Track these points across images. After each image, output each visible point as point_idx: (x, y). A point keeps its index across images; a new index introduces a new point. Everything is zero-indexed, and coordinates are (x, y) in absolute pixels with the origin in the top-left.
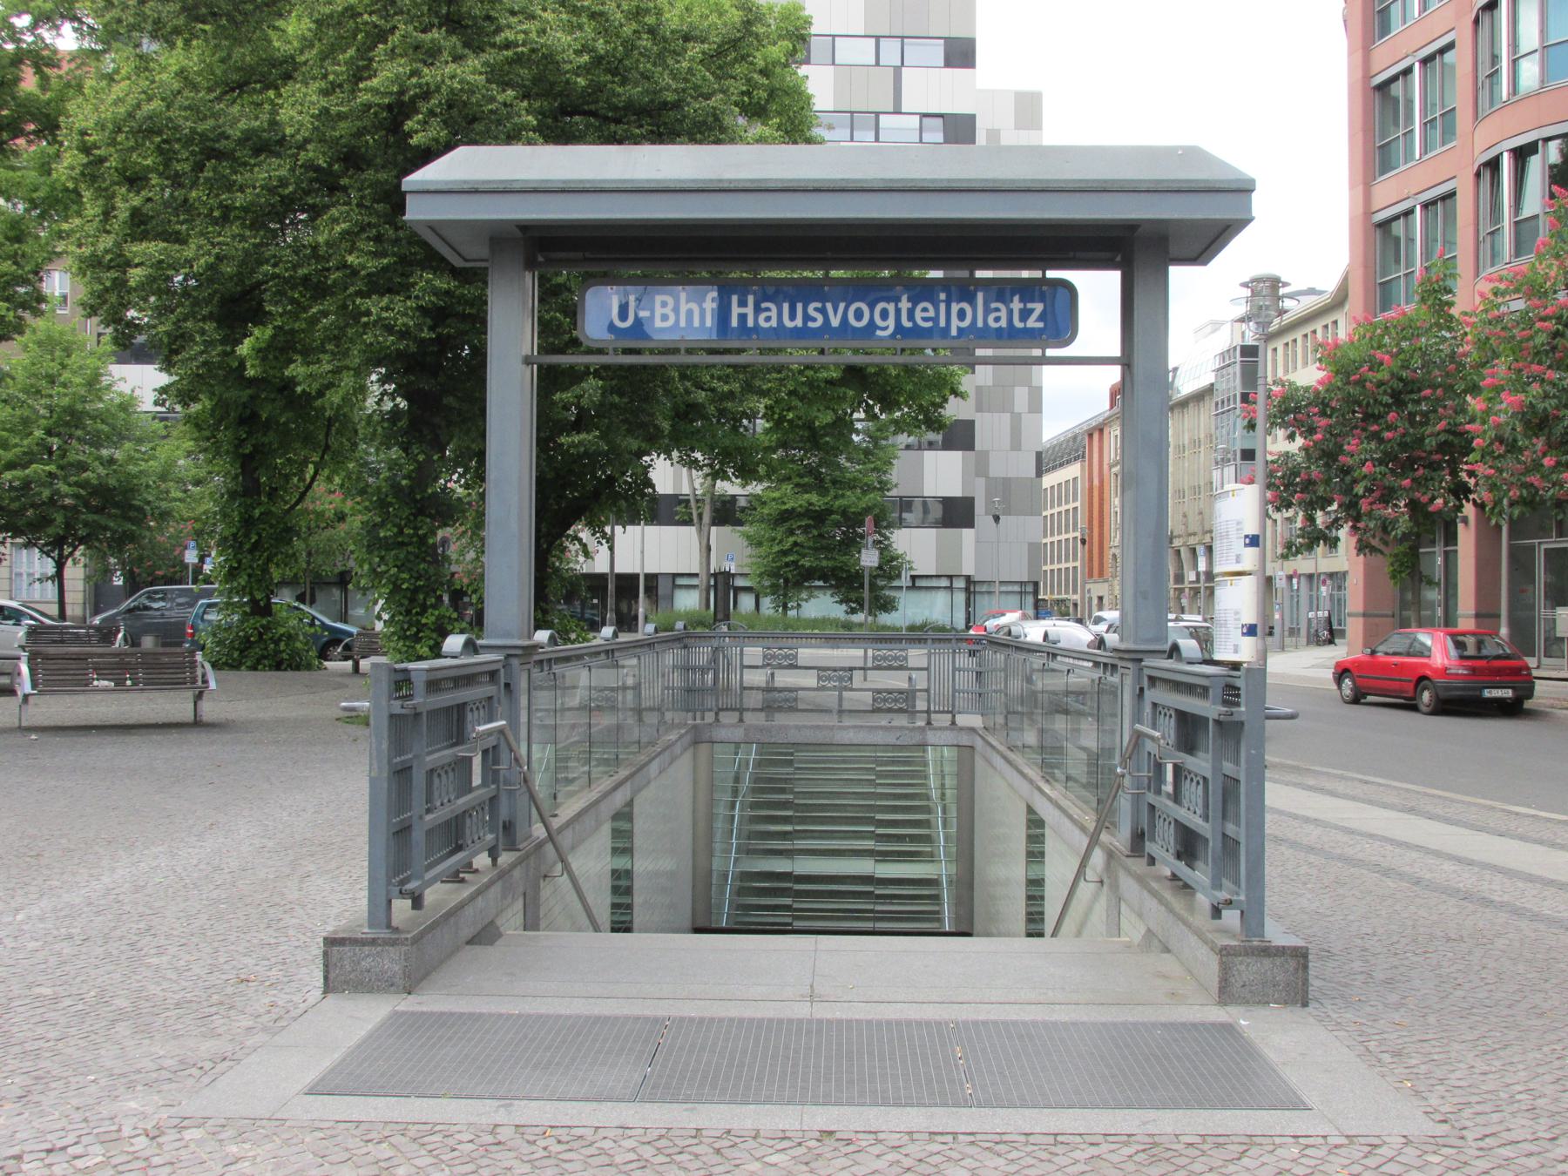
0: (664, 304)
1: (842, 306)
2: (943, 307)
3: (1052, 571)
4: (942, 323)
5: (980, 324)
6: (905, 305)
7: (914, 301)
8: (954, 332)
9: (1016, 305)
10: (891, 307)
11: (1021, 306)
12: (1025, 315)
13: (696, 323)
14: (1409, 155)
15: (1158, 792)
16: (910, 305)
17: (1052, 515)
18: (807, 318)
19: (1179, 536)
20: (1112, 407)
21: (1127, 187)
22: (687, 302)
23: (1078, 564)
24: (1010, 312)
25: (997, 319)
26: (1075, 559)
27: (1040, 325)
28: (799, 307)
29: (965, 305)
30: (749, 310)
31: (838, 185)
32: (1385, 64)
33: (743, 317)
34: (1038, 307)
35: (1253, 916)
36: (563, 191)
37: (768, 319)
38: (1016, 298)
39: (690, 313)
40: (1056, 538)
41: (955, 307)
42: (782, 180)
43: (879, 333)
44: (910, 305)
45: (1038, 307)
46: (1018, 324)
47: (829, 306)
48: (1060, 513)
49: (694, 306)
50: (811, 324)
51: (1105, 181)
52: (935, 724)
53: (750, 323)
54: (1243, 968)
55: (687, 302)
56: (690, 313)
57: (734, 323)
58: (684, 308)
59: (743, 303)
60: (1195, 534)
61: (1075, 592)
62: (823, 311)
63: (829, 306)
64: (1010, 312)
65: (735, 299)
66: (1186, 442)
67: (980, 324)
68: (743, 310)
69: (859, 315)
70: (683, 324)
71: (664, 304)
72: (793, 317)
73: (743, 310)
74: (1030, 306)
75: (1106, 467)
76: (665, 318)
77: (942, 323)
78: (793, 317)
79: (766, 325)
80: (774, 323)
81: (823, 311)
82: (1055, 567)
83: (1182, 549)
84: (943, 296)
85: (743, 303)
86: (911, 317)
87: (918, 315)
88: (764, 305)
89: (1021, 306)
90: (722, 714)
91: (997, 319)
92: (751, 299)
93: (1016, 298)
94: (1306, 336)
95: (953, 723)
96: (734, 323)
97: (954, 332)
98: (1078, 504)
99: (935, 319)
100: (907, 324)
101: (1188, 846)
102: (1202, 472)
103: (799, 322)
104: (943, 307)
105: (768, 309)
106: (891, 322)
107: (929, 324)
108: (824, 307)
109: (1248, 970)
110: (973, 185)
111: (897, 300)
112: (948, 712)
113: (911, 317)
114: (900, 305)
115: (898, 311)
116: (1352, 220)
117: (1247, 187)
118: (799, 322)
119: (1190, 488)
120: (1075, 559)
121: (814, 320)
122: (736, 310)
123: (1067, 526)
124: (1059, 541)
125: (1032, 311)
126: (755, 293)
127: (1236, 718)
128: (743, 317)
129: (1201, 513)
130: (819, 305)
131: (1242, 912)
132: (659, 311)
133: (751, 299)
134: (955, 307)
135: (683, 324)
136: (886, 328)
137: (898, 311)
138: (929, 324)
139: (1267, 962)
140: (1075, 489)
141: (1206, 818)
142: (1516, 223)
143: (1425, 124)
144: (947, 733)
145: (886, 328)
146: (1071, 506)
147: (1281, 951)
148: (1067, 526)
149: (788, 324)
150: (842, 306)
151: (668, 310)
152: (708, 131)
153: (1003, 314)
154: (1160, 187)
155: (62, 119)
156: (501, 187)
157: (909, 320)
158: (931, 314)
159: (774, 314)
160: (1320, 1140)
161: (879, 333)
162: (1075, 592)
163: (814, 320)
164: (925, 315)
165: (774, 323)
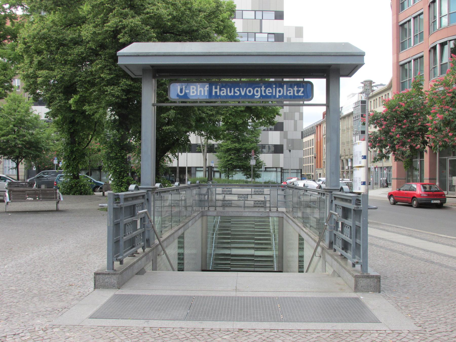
0: (193, 89)
1: (245, 89)
2: (274, 89)
3: (306, 166)
4: (274, 94)
5: (285, 94)
6: (263, 89)
7: (266, 87)
8: (277, 97)
9: (296, 89)
10: (259, 89)
11: (297, 89)
12: (298, 91)
13: (203, 94)
14: (410, 45)
15: (337, 230)
16: (265, 89)
17: (306, 150)
18: (235, 92)
19: (343, 156)
20: (323, 118)
21: (328, 54)
22: (200, 88)
23: (313, 164)
24: (294, 91)
25: (290, 93)
26: (313, 163)
27: (303, 94)
28: (232, 89)
29: (281, 89)
30: (218, 90)
31: (244, 54)
32: (403, 19)
33: (216, 92)
34: (302, 89)
35: (364, 266)
36: (164, 56)
37: (223, 93)
38: (296, 87)
39: (201, 91)
40: (307, 157)
41: (278, 89)
42: (227, 52)
43: (256, 97)
44: (265, 89)
45: (302, 89)
46: (296, 94)
47: (241, 89)
48: (308, 149)
49: (202, 89)
50: (236, 94)
51: (321, 53)
52: (272, 210)
53: (218, 94)
54: (361, 281)
55: (200, 88)
56: (201, 91)
57: (214, 94)
58: (199, 90)
59: (216, 88)
60: (347, 155)
61: (313, 172)
62: (239, 90)
63: (241, 89)
64: (294, 91)
65: (214, 87)
66: (345, 129)
67: (285, 94)
68: (216, 90)
69: (250, 92)
70: (199, 94)
71: (193, 89)
72: (230, 92)
73: (216, 90)
74: (299, 89)
75: (322, 136)
76: (193, 92)
77: (274, 94)
78: (230, 92)
79: (223, 95)
80: (225, 94)
81: (239, 90)
82: (307, 165)
83: (344, 160)
84: (274, 86)
85: (216, 88)
86: (265, 92)
87: (267, 92)
88: (222, 89)
89: (297, 89)
90: (210, 208)
91: (290, 93)
92: (218, 87)
93: (296, 87)
94: (380, 98)
95: (277, 210)
96: (214, 94)
97: (277, 97)
98: (313, 147)
99: (272, 93)
100: (264, 94)
101: (346, 246)
102: (350, 137)
103: (232, 94)
104: (274, 89)
105: (223, 90)
106: (259, 94)
107: (270, 94)
108: (240, 89)
109: (363, 282)
110: (283, 54)
111: (261, 87)
112: (276, 207)
113: (265, 92)
114: (262, 89)
115: (261, 90)
116: (393, 64)
117: (363, 54)
118: (232, 94)
119: (346, 142)
120: (313, 163)
121: (237, 93)
122: (214, 90)
123: (310, 153)
124: (308, 157)
125: (300, 90)
126: (219, 85)
127: (359, 209)
128: (216, 92)
129: (349, 149)
130: (238, 89)
131: (361, 265)
132: (192, 90)
133: (218, 87)
134: (278, 89)
135: (199, 94)
136: (258, 95)
137: (261, 90)
138: (270, 94)
139: (368, 280)
140: (313, 142)
141: (351, 238)
142: (441, 65)
143: (415, 36)
144: (276, 213)
145: (258, 95)
146: (311, 147)
147: (373, 277)
148: (310, 153)
149: (229, 94)
150: (245, 89)
151: (194, 90)
152: (206, 38)
153: (292, 91)
154: (337, 54)
155: (18, 35)
156: (146, 54)
157: (264, 93)
158: (271, 91)
159: (225, 91)
160: (384, 332)
161: (256, 97)
162: (313, 172)
163: (237, 93)
164: (269, 92)
165: (225, 94)
